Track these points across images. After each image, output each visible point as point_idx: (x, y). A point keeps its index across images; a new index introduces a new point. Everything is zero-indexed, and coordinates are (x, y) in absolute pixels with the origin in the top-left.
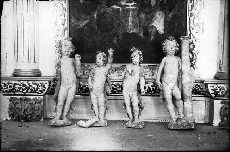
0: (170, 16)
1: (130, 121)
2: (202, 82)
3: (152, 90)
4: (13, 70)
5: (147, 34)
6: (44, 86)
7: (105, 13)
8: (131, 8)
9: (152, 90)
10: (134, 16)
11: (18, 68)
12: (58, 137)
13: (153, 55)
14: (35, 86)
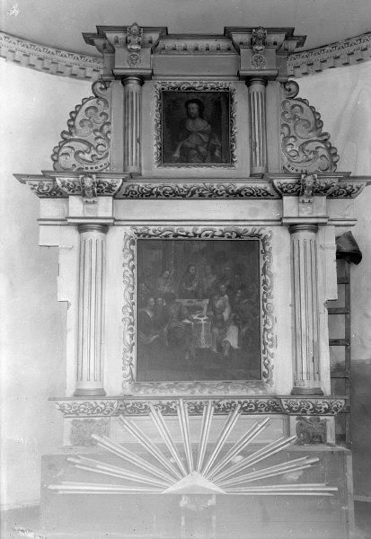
0: (244, 330)
1: (339, 208)
2: (276, 397)
3: (51, 487)
4: (74, 390)
5: (220, 349)
6: (112, 405)
7: (176, 327)
8: (203, 322)
9: (51, 487)
10: (207, 331)
11: (82, 387)
12: (265, 380)
13: (210, 501)
14: (102, 406)
